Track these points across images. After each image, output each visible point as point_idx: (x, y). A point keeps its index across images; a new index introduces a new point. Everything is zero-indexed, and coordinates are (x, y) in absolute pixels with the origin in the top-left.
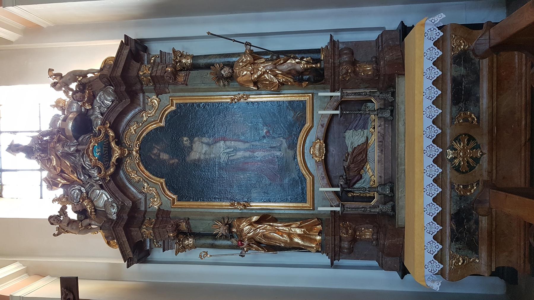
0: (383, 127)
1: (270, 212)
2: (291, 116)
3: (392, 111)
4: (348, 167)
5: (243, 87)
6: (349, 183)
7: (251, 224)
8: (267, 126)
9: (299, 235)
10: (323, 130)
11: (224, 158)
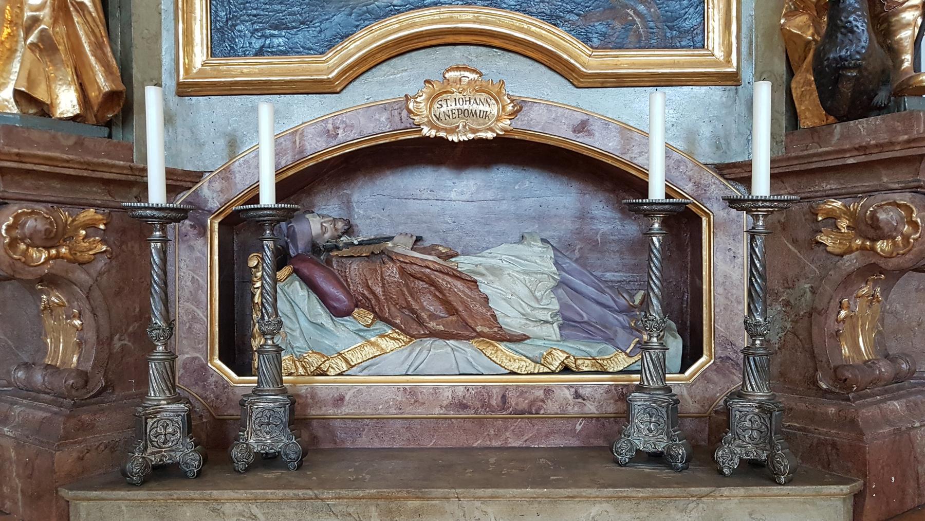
0: (573, 410)
3: (656, 458)
4: (390, 256)
6: (311, 263)
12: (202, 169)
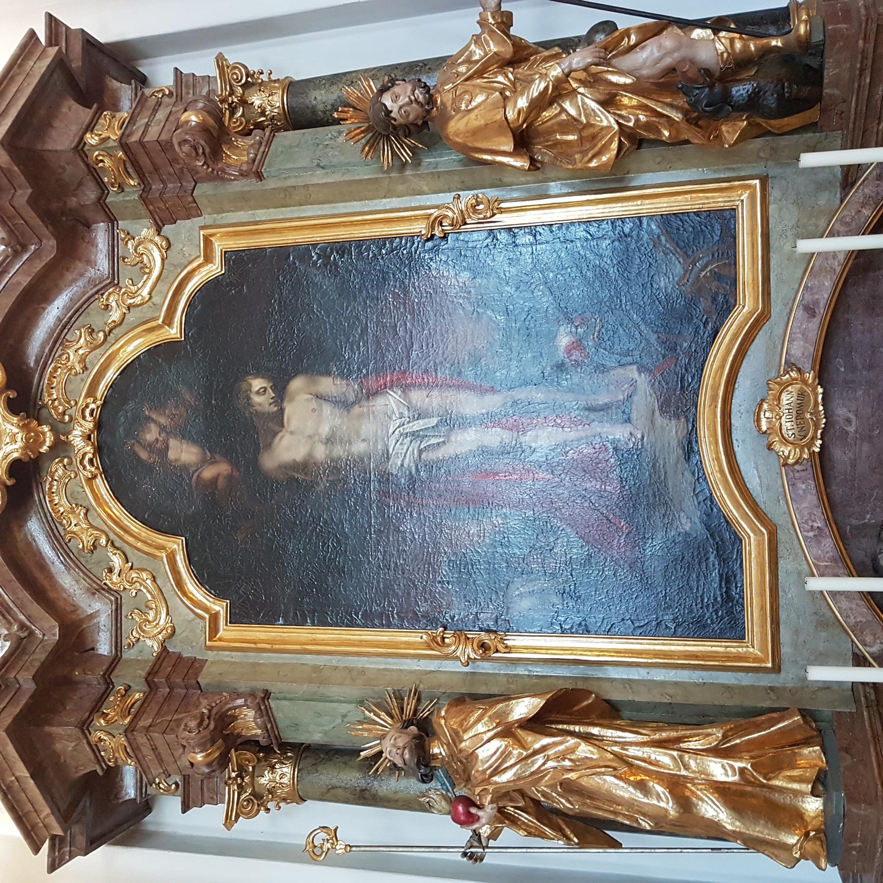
1: (591, 672)
2: (670, 276)
5: (475, 167)
7: (507, 732)
8: (571, 321)
9: (722, 790)
10: (814, 328)
11: (402, 457)
12: (851, 653)
